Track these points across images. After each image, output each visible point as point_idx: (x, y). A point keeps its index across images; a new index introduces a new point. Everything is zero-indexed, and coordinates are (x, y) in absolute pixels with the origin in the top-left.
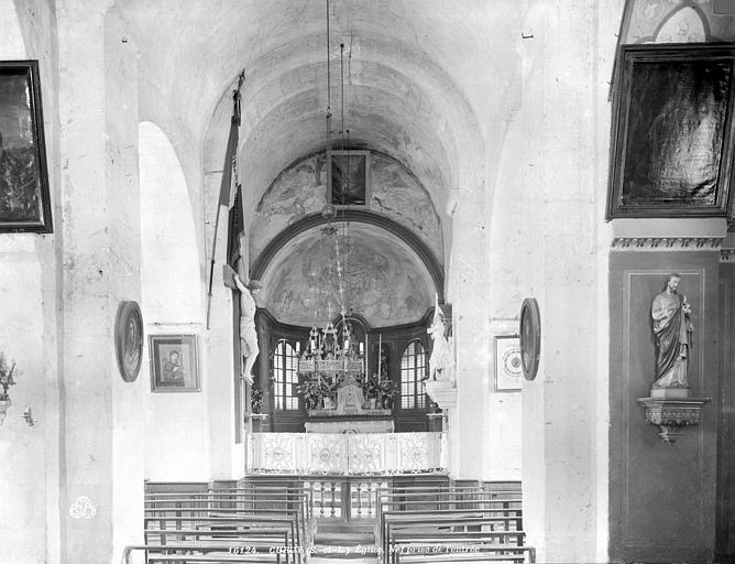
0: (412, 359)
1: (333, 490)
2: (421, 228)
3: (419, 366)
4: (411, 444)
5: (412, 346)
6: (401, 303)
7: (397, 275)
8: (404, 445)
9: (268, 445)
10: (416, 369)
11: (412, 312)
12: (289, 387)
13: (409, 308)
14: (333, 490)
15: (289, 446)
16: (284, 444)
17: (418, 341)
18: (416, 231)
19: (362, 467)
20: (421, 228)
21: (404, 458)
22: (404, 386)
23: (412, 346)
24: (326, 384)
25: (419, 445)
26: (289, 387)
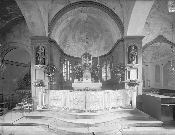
0: (105, 66)
1: (151, 30)
2: (115, 10)
3: (108, 71)
4: (115, 95)
5: (105, 62)
6: (102, 49)
7: (101, 39)
8: (113, 96)
9: (52, 95)
10: (107, 72)
11: (105, 51)
12: (69, 74)
13: (104, 50)
14: (151, 30)
15: (60, 96)
16: (58, 95)
17: (108, 60)
18: (113, 10)
19: (94, 107)
20: (115, 10)
21: (113, 102)
22: (103, 74)
23: (105, 62)
24: (79, 42)
25: (119, 95)
26: (69, 74)
